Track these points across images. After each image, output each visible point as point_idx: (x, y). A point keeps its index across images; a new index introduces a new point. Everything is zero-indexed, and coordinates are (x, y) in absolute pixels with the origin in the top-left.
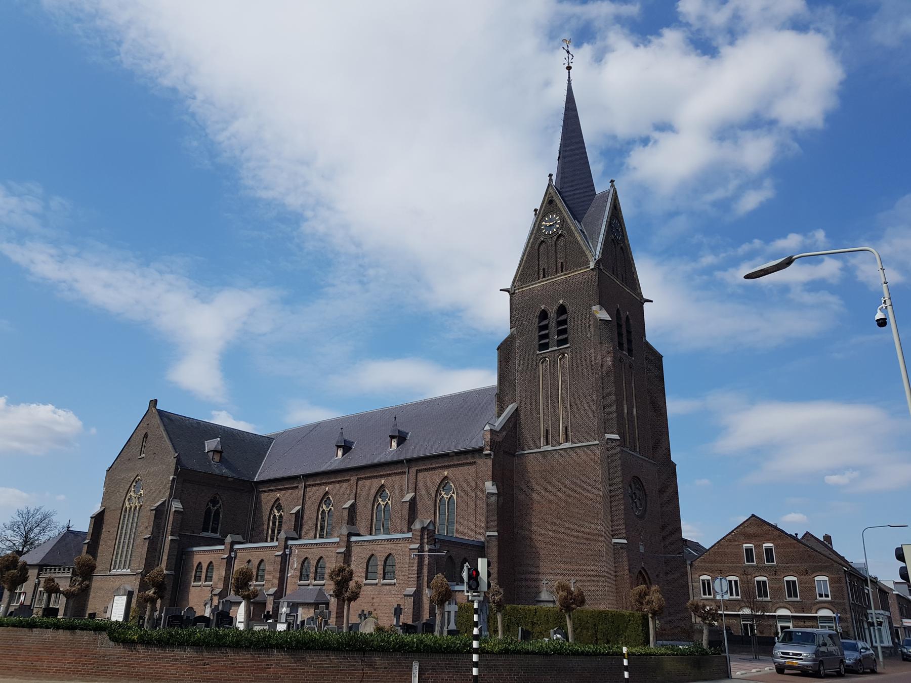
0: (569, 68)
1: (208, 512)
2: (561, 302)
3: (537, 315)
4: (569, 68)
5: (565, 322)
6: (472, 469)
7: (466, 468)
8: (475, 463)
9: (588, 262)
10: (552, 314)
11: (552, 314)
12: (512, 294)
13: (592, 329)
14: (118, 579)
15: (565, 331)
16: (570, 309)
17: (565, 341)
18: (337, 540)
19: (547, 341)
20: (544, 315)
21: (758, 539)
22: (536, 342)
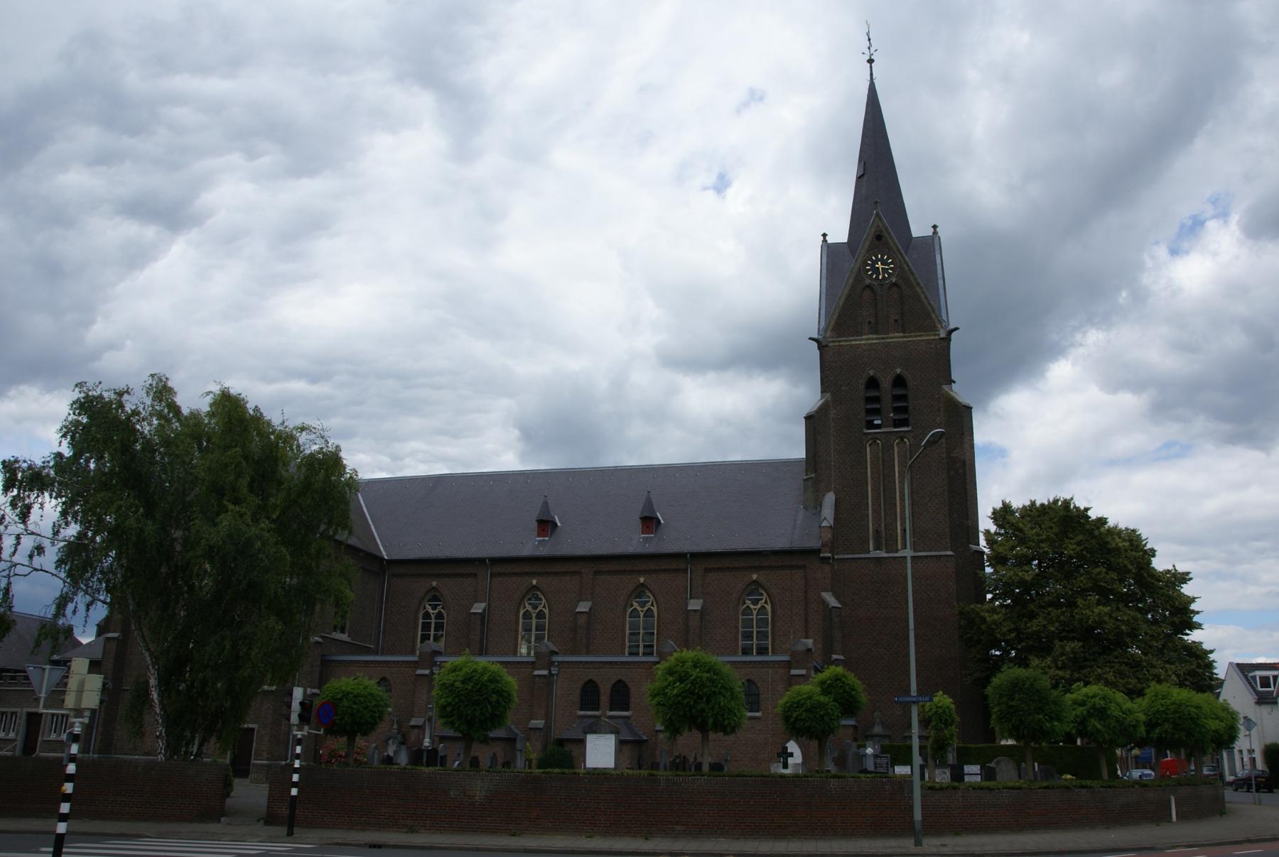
0: (871, 61)
2: (898, 371)
3: (863, 381)
4: (871, 61)
10: (886, 383)
11: (886, 383)
15: (905, 410)
17: (904, 423)
20: (872, 383)
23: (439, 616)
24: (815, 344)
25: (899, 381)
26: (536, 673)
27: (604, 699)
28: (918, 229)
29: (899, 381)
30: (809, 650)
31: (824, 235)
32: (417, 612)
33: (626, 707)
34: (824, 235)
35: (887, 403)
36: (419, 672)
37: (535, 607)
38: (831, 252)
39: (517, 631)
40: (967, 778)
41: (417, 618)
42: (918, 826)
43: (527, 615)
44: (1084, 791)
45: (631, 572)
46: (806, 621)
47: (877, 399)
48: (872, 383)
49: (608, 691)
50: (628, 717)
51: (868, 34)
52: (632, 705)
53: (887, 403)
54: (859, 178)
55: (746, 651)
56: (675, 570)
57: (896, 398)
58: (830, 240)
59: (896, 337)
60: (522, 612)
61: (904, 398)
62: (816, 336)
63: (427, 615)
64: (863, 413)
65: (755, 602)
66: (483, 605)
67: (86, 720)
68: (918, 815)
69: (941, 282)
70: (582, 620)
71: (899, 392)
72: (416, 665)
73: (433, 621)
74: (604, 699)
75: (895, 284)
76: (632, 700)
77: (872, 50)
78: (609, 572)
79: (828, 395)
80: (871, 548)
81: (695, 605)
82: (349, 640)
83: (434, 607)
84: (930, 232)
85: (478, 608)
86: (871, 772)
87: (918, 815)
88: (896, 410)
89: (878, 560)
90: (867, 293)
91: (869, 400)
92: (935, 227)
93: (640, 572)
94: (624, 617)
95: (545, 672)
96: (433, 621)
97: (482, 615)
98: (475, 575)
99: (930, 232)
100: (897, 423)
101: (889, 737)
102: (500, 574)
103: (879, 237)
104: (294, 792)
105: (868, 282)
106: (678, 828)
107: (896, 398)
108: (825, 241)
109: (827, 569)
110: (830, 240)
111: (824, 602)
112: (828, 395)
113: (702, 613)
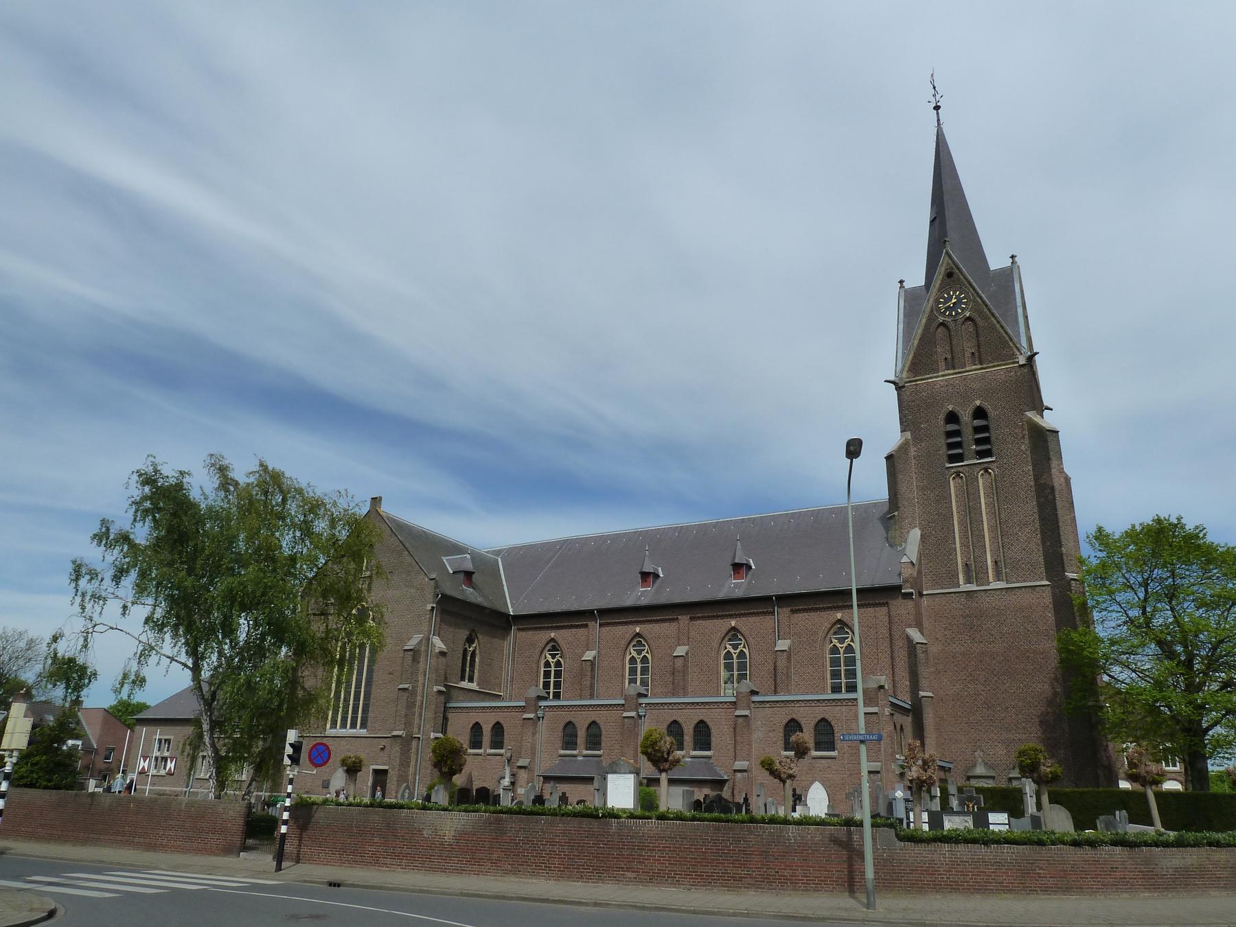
0: (937, 108)
1: (465, 651)
2: (978, 403)
3: (942, 417)
4: (937, 108)
5: (985, 429)
6: (674, 625)
7: (871, 610)
8: (586, 626)
9: (1013, 356)
10: (966, 416)
11: (966, 416)
12: (899, 388)
13: (1027, 441)
14: (343, 742)
15: (987, 441)
16: (992, 413)
17: (988, 453)
18: (622, 702)
19: (960, 451)
20: (952, 418)
21: (321, 762)
22: (944, 451)
23: (558, 664)
24: (893, 386)
25: (980, 413)
26: (626, 714)
27: (688, 739)
28: (996, 261)
30: (882, 687)
31: (901, 282)
32: (538, 662)
33: (707, 747)
34: (901, 282)
35: (968, 436)
36: (526, 716)
37: (639, 652)
38: (911, 299)
39: (623, 676)
40: (991, 827)
42: (870, 885)
43: (547, 664)
44: (1118, 849)
45: (723, 617)
46: (892, 658)
47: (957, 433)
48: (952, 418)
49: (691, 731)
50: (710, 757)
51: (932, 83)
52: (713, 744)
53: (968, 436)
54: (932, 222)
55: (836, 689)
56: (763, 613)
57: (977, 430)
58: (907, 285)
59: (973, 371)
60: (628, 658)
61: (985, 429)
62: (892, 378)
63: (547, 664)
64: (945, 446)
65: (842, 641)
66: (788, 642)
68: (870, 873)
69: (1020, 311)
70: (679, 663)
71: (978, 423)
72: (523, 709)
73: (735, 661)
74: (688, 739)
75: (969, 319)
76: (713, 739)
77: (938, 97)
78: (703, 618)
79: (908, 435)
80: (991, 579)
81: (782, 645)
82: (477, 688)
83: (553, 656)
84: (1008, 263)
85: (589, 655)
87: (870, 873)
88: (978, 442)
89: (969, 593)
90: (941, 329)
91: (949, 434)
92: (1013, 257)
93: (731, 616)
94: (718, 659)
95: (633, 714)
96: (735, 661)
97: (592, 663)
98: (586, 626)
99: (1008, 263)
100: (981, 454)
101: (993, 778)
103: (950, 275)
104: (284, 829)
105: (941, 319)
106: (629, 874)
108: (902, 287)
109: (910, 604)
110: (907, 285)
111: (909, 639)
112: (908, 435)
113: (788, 653)
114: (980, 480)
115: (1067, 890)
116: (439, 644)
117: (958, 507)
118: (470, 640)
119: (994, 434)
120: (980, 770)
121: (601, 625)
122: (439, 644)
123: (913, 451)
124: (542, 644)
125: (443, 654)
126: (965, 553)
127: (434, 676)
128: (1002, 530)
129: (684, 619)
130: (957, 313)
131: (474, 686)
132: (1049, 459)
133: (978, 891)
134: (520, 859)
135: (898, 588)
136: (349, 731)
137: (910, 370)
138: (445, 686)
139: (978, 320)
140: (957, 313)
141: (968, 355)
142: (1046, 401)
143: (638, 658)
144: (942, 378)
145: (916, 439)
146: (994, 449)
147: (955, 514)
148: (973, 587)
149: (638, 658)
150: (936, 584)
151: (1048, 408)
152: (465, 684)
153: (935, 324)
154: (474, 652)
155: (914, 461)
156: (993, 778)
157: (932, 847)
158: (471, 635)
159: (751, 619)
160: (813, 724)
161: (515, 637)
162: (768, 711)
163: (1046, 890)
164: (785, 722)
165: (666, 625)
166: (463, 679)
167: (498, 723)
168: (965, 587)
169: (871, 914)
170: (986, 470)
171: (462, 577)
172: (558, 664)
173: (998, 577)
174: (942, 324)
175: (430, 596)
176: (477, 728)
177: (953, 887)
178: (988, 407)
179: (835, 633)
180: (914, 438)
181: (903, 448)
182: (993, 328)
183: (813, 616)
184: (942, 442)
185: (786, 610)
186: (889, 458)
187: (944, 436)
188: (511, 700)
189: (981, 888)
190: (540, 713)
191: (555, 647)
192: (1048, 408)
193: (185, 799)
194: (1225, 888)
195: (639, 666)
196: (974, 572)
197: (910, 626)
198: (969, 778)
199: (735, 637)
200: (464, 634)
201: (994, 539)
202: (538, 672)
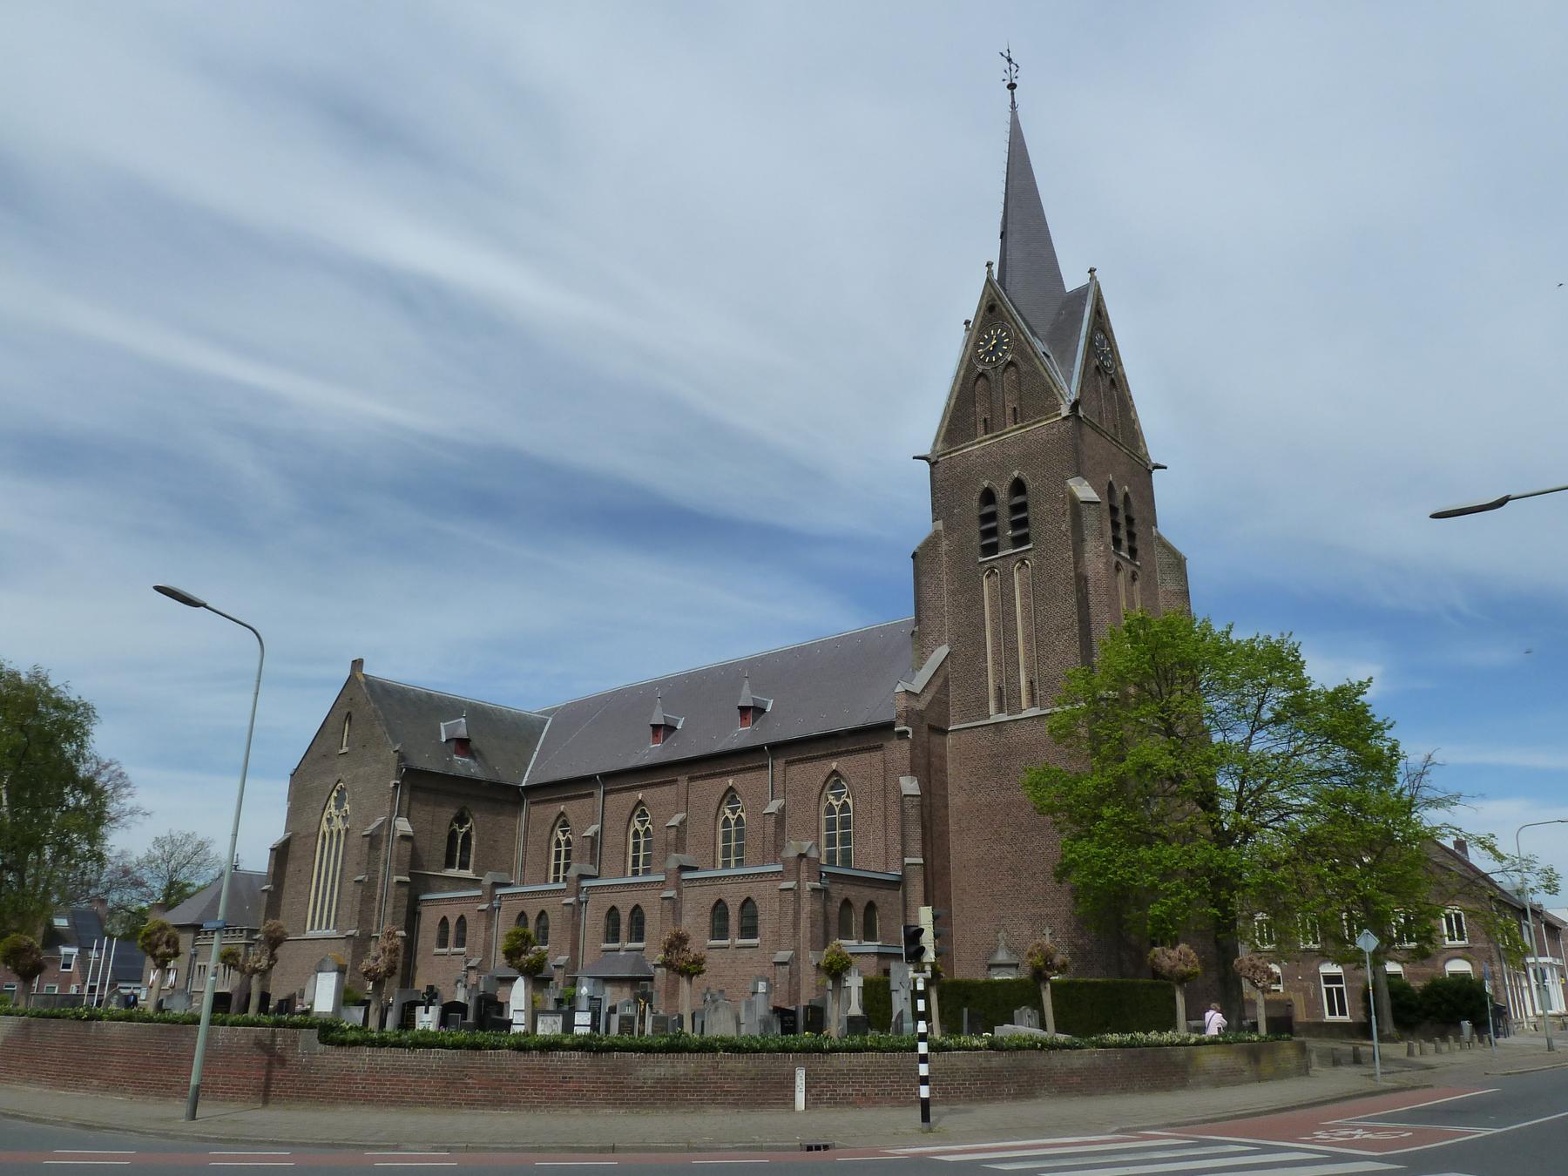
0: (1012, 86)
1: (452, 836)
2: (1016, 474)
3: (977, 496)
4: (1012, 86)
5: (1022, 507)
10: (1002, 494)
11: (1002, 494)
13: (1068, 518)
14: (318, 944)
16: (1031, 486)
20: (988, 497)
23: (568, 843)
29: (1018, 487)
33: (640, 940)
39: (626, 854)
41: (549, 848)
47: (991, 517)
52: (761, 930)
59: (1012, 432)
60: (824, 806)
61: (1022, 507)
62: (927, 451)
63: (830, 810)
67: (929, 975)
71: (1018, 500)
75: (1011, 363)
79: (940, 525)
80: (1024, 705)
86: (150, 1020)
88: (1016, 525)
92: (1091, 271)
93: (728, 774)
97: (593, 839)
101: (1017, 966)
102: (612, 791)
105: (980, 368)
106: (95, 1082)
107: (991, 517)
114: (1016, 576)
115: (497, 1103)
116: (403, 826)
117: (992, 613)
118: (461, 819)
119: (1031, 514)
120: (1002, 957)
121: (605, 793)
122: (403, 826)
123: (944, 545)
124: (552, 821)
125: (405, 838)
126: (998, 673)
127: (394, 864)
128: (1038, 641)
129: (683, 780)
130: (998, 358)
131: (468, 874)
132: (1083, 540)
133: (393, 1103)
134: (76, 1070)
135: (890, 726)
136: (324, 933)
137: (944, 440)
138: (410, 875)
139: (1021, 363)
140: (998, 358)
141: (1009, 411)
142: (1155, 458)
143: (641, 830)
144: (978, 446)
145: (949, 528)
146: (1032, 535)
147: (988, 622)
148: (1004, 717)
149: (641, 830)
150: (966, 717)
151: (1157, 467)
152: (453, 872)
153: (975, 375)
154: (467, 836)
155: (945, 558)
156: (1017, 966)
157: (352, 1050)
158: (462, 814)
159: (749, 776)
160: (739, 904)
161: (528, 813)
162: (697, 891)
163: (472, 1103)
164: (713, 903)
165: (666, 788)
166: (450, 864)
167: (613, 908)
168: (996, 718)
169: (195, 1127)
170: (992, 569)
171: (453, 744)
172: (568, 843)
173: (1033, 703)
174: (981, 375)
175: (393, 772)
176: (720, 909)
177: (369, 1099)
178: (1026, 477)
179: (832, 788)
180: (948, 528)
181: (931, 543)
182: (1036, 373)
183: (809, 767)
184: (975, 529)
185: (781, 762)
186: (914, 556)
187: (977, 522)
188: (523, 884)
189: (397, 1100)
190: (582, 897)
191: (563, 821)
192: (1157, 467)
193: (1418, 984)
194: (735, 1104)
195: (642, 840)
196: (1006, 699)
197: (904, 774)
198: (991, 966)
199: (733, 800)
200: (449, 813)
201: (1028, 651)
202: (549, 853)
